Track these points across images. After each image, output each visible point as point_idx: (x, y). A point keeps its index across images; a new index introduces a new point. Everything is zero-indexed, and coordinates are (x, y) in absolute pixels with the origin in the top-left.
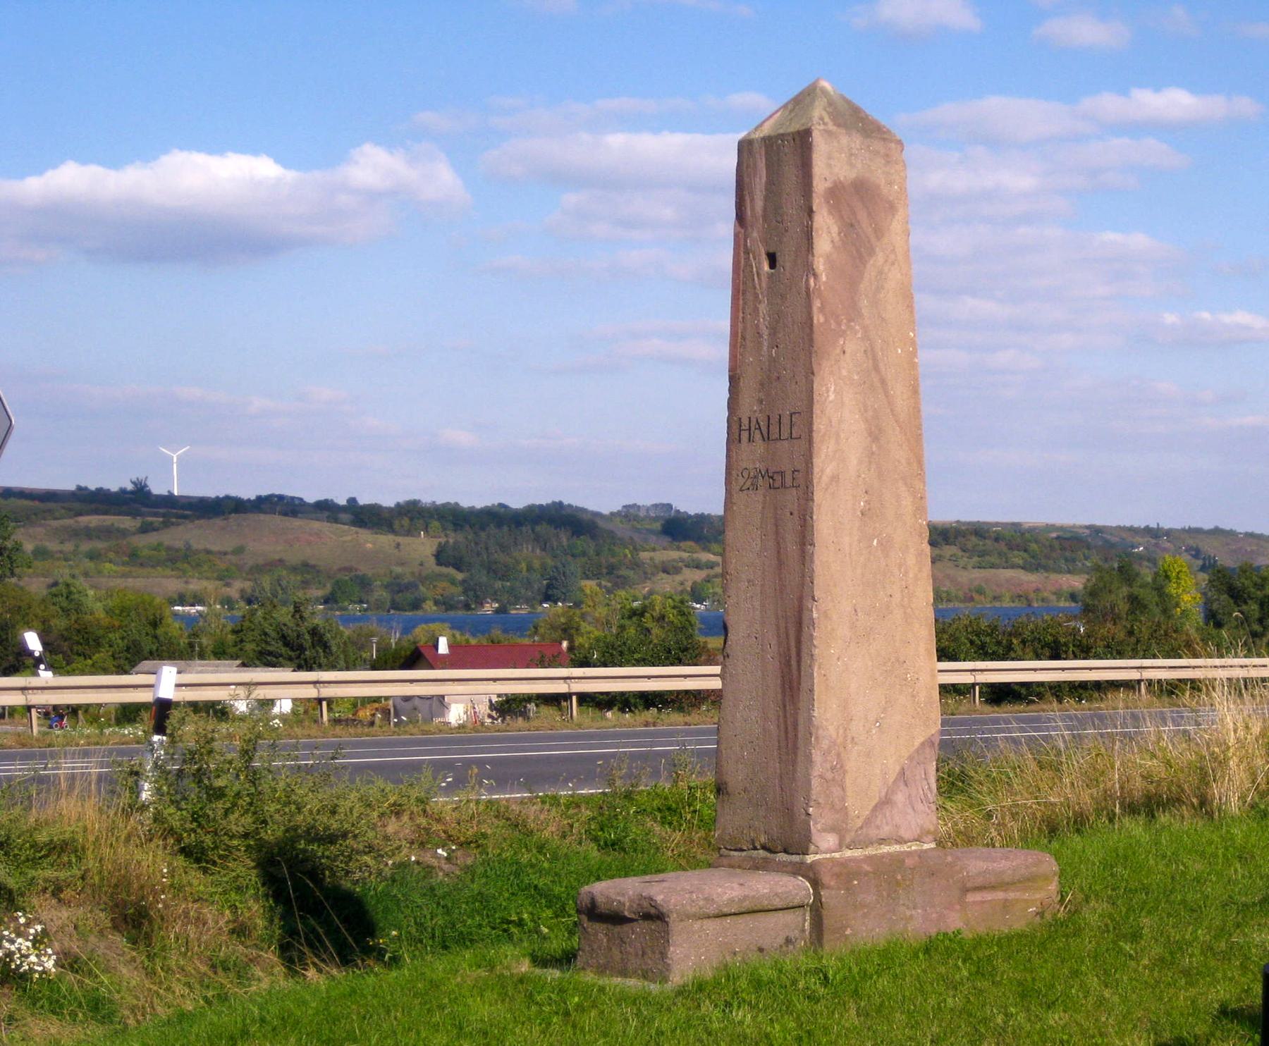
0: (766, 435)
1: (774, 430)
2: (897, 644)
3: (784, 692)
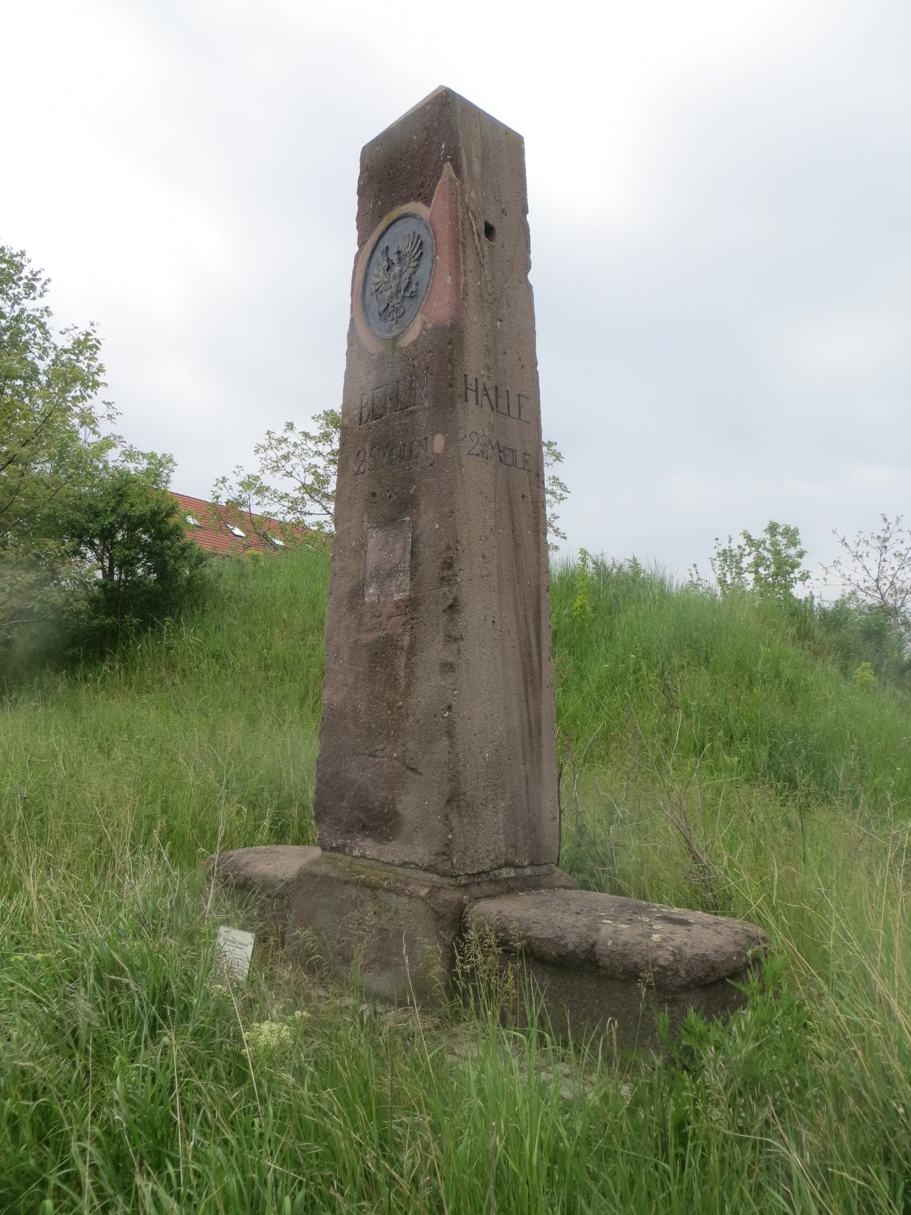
0: (493, 402)
1: (503, 403)
3: (526, 684)
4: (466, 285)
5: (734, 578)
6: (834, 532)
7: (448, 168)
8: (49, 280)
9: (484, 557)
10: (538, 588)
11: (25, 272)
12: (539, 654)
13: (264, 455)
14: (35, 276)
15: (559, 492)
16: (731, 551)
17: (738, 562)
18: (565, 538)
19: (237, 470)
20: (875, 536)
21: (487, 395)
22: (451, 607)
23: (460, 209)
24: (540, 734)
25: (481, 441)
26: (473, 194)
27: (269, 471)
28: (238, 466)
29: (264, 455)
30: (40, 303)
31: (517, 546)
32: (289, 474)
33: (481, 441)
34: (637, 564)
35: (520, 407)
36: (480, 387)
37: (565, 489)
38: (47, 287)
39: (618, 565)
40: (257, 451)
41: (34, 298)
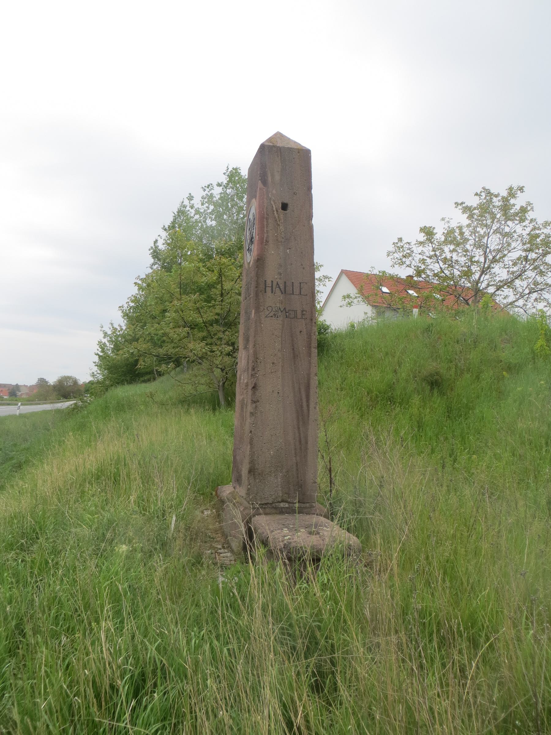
1: (289, 289)
4: (268, 237)
9: (273, 363)
10: (309, 375)
12: (308, 406)
13: (392, 257)
21: (279, 287)
22: (254, 387)
24: (307, 443)
25: (274, 310)
26: (274, 192)
27: (398, 265)
28: (372, 267)
29: (392, 257)
33: (274, 310)
36: (275, 284)
40: (388, 255)
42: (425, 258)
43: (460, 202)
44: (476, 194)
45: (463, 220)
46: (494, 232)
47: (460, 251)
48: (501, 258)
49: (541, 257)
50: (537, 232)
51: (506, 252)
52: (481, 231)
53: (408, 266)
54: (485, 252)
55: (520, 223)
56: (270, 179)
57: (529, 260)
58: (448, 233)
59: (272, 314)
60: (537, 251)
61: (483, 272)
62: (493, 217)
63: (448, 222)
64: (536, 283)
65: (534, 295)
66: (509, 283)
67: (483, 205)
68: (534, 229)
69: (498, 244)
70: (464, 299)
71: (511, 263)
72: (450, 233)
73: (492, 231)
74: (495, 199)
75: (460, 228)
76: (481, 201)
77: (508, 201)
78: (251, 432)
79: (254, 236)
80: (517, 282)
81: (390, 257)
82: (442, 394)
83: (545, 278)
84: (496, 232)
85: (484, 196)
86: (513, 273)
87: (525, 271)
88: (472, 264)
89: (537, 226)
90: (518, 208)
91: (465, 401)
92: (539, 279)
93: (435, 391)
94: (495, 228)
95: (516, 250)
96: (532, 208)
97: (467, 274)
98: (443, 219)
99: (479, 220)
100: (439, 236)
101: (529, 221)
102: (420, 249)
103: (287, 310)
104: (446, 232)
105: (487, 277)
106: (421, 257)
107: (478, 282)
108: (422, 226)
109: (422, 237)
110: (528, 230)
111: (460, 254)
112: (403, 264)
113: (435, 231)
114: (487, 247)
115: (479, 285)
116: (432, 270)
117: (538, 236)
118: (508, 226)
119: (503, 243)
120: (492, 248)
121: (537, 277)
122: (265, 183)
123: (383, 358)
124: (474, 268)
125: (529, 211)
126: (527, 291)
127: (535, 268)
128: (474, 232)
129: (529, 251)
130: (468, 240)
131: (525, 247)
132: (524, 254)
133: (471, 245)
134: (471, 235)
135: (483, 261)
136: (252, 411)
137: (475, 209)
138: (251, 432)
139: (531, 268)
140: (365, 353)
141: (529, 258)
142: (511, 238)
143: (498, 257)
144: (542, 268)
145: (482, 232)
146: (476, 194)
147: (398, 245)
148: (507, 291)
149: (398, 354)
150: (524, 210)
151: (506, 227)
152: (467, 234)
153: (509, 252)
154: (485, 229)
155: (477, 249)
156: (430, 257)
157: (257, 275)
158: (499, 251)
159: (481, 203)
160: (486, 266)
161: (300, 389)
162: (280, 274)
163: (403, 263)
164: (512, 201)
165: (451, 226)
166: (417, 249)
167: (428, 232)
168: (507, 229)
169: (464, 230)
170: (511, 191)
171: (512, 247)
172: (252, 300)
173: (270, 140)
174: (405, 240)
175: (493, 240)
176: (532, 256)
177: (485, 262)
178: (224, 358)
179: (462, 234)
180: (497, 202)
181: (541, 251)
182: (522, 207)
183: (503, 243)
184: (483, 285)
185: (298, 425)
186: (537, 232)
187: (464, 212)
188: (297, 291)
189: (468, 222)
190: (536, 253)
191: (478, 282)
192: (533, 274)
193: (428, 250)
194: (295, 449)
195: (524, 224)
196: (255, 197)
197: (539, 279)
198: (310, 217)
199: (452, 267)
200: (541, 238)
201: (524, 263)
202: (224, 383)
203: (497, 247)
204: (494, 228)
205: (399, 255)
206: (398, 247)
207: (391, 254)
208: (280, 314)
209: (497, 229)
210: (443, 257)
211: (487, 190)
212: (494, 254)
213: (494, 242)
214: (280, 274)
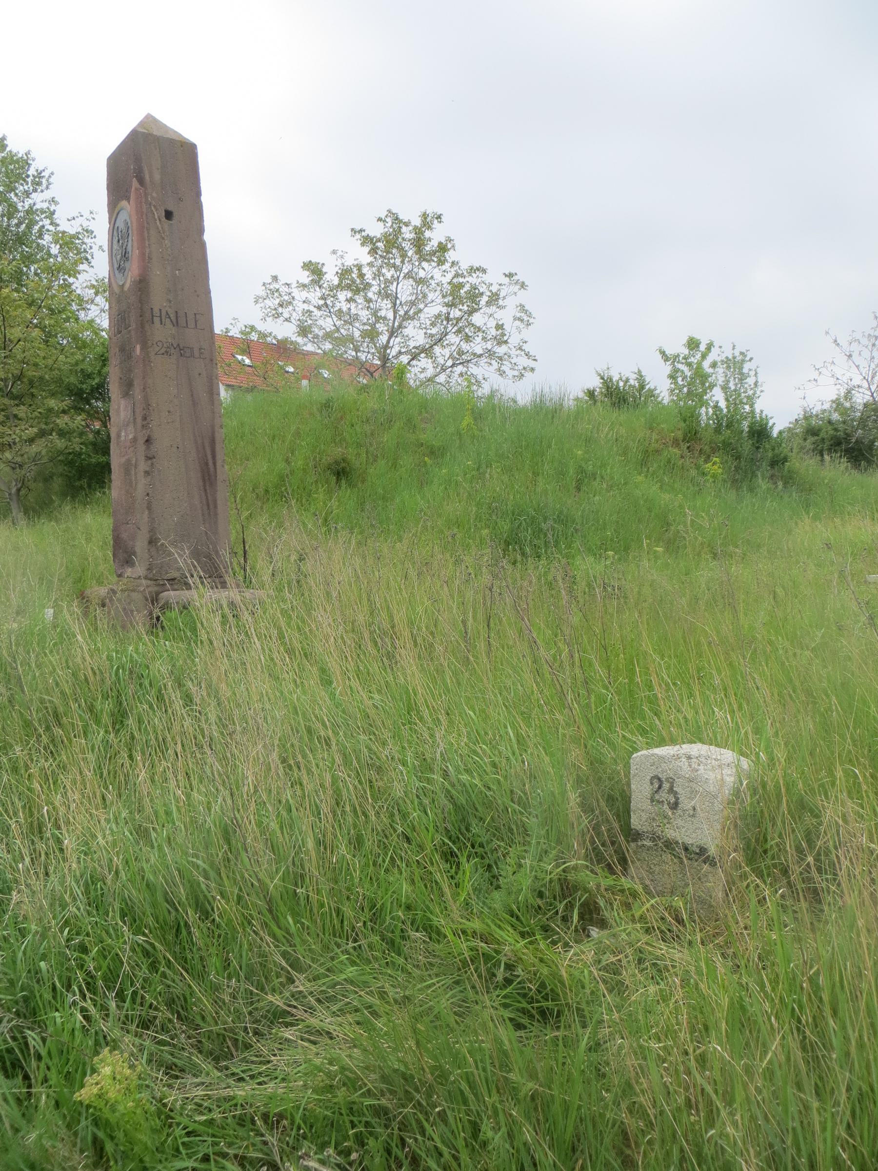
0: (174, 321)
1: (182, 321)
2: (715, 1047)
3: (204, 481)
4: (150, 253)
5: (736, 385)
6: (827, 333)
7: (135, 183)
8: (52, 173)
9: (169, 412)
10: (213, 427)
11: (32, 172)
12: (215, 464)
13: (262, 305)
14: (39, 174)
15: (526, 318)
16: (734, 358)
17: (741, 368)
18: (535, 360)
19: (233, 322)
20: (866, 334)
21: (169, 318)
22: (147, 441)
23: (144, 206)
24: (216, 507)
25: (165, 345)
26: (154, 195)
27: (271, 318)
28: (234, 319)
29: (262, 305)
30: (47, 195)
31: (195, 404)
32: (287, 320)
33: (165, 345)
34: (641, 376)
35: (196, 321)
36: (164, 313)
37: (530, 316)
38: (51, 180)
39: (624, 379)
40: (256, 302)
41: (42, 191)
42: (312, 308)
43: (358, 228)
44: (380, 219)
45: (362, 255)
46: (405, 277)
47: (359, 301)
48: (416, 313)
49: (466, 316)
50: (461, 280)
51: (421, 306)
52: (389, 274)
53: (286, 320)
54: (395, 304)
55: (438, 265)
56: (147, 177)
57: (451, 320)
58: (341, 274)
59: (163, 351)
60: (461, 307)
61: (392, 333)
62: (404, 256)
63: (342, 257)
64: (461, 353)
65: (459, 369)
66: (427, 351)
67: (390, 235)
68: (457, 275)
69: (412, 294)
70: (368, 371)
71: (428, 323)
72: (344, 273)
73: (402, 275)
74: (404, 229)
75: (359, 267)
76: (386, 230)
77: (422, 233)
78: (148, 494)
79: (129, 249)
80: (437, 350)
81: (259, 305)
82: (351, 485)
83: (472, 344)
84: (408, 276)
85: (389, 224)
86: (432, 336)
87: (447, 334)
88: (377, 321)
89: (460, 272)
90: (436, 245)
91: (380, 491)
92: (465, 346)
93: (343, 482)
94: (406, 271)
95: (434, 304)
96: (453, 246)
97: (371, 334)
98: (334, 252)
99: (384, 258)
100: (331, 277)
101: (450, 264)
102: (304, 294)
103: (181, 346)
104: (340, 271)
105: (398, 340)
106: (306, 307)
107: (386, 347)
108: (307, 260)
109: (305, 277)
110: (449, 277)
111: (360, 306)
112: (279, 317)
113: (324, 270)
114: (397, 298)
115: (388, 351)
116: (321, 328)
117: (461, 286)
118: (423, 269)
119: (417, 293)
120: (403, 301)
121: (462, 343)
122: (141, 181)
123: (269, 443)
124: (381, 327)
125: (449, 250)
126: (450, 363)
127: (459, 331)
128: (378, 274)
129: (451, 306)
130: (369, 285)
131: (446, 300)
132: (444, 310)
133: (374, 293)
134: (374, 278)
135: (392, 318)
136: (148, 469)
137: (379, 240)
138: (148, 494)
139: (453, 330)
140: (242, 437)
141: (451, 316)
142: (428, 287)
143: (411, 312)
144: (467, 330)
145: (388, 275)
146: (380, 219)
147: (272, 287)
148: (424, 362)
149: (289, 437)
150: (442, 248)
151: (421, 271)
152: (369, 276)
153: (426, 306)
154: (392, 271)
155: (382, 300)
156: (319, 308)
157: (141, 301)
158: (413, 303)
159: (386, 233)
160: (396, 324)
161: (203, 443)
162: (170, 301)
163: (277, 316)
164: (428, 234)
165: (346, 264)
166: (300, 295)
167: (315, 270)
168: (422, 274)
169: (365, 270)
170: (426, 218)
171: (429, 299)
172: (133, 333)
173: (142, 124)
174: (282, 280)
175: (405, 287)
176: (455, 313)
177: (395, 318)
178: (24, 447)
179: (361, 276)
180: (407, 233)
181: (465, 308)
182: (440, 243)
183: (417, 293)
184: (393, 352)
185: (205, 486)
186: (461, 280)
187: (363, 244)
188: (191, 324)
189: (370, 259)
190: (460, 310)
191: (386, 347)
192: (457, 340)
193: (314, 296)
194: (203, 515)
195: (444, 267)
196: (128, 199)
197: (465, 346)
198: (201, 230)
199: (351, 324)
200: (465, 289)
201: (445, 322)
202: (19, 490)
203: (410, 298)
204: (405, 270)
205: (273, 302)
206: (270, 290)
207: (261, 300)
208: (173, 351)
209: (408, 273)
210: (336, 309)
211: (394, 214)
212: (406, 308)
213: (405, 290)
214: (170, 301)
